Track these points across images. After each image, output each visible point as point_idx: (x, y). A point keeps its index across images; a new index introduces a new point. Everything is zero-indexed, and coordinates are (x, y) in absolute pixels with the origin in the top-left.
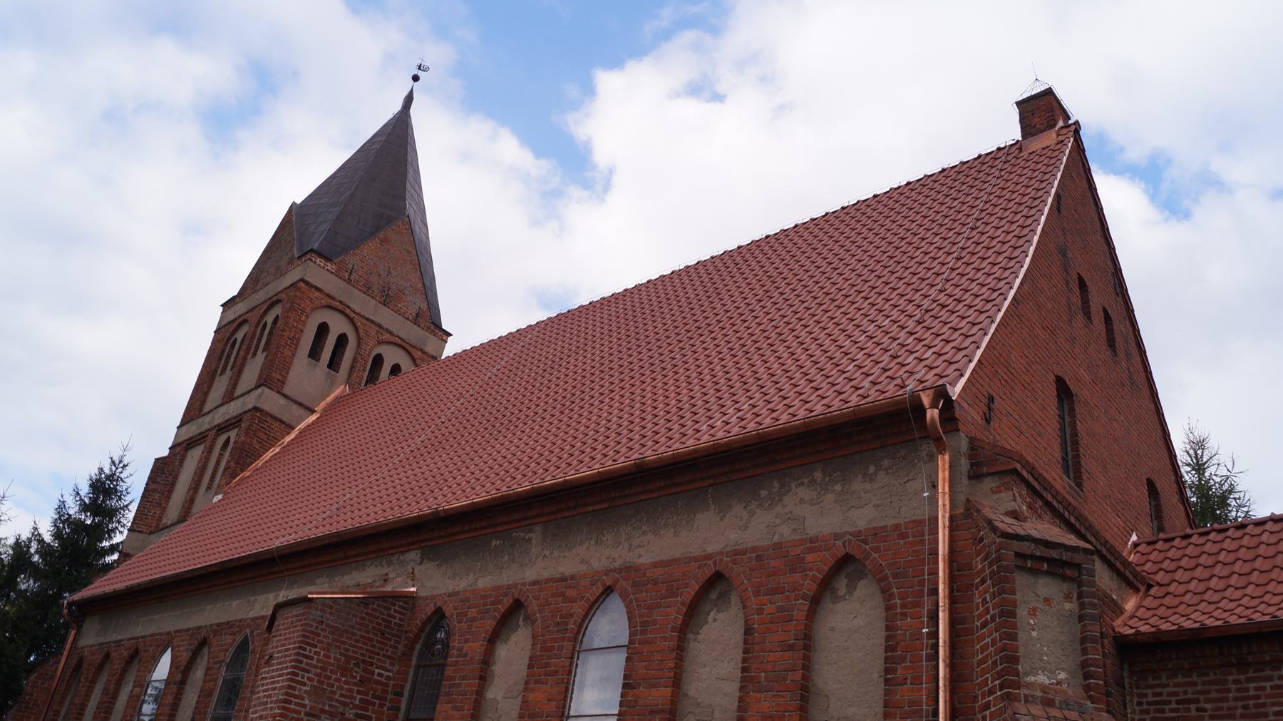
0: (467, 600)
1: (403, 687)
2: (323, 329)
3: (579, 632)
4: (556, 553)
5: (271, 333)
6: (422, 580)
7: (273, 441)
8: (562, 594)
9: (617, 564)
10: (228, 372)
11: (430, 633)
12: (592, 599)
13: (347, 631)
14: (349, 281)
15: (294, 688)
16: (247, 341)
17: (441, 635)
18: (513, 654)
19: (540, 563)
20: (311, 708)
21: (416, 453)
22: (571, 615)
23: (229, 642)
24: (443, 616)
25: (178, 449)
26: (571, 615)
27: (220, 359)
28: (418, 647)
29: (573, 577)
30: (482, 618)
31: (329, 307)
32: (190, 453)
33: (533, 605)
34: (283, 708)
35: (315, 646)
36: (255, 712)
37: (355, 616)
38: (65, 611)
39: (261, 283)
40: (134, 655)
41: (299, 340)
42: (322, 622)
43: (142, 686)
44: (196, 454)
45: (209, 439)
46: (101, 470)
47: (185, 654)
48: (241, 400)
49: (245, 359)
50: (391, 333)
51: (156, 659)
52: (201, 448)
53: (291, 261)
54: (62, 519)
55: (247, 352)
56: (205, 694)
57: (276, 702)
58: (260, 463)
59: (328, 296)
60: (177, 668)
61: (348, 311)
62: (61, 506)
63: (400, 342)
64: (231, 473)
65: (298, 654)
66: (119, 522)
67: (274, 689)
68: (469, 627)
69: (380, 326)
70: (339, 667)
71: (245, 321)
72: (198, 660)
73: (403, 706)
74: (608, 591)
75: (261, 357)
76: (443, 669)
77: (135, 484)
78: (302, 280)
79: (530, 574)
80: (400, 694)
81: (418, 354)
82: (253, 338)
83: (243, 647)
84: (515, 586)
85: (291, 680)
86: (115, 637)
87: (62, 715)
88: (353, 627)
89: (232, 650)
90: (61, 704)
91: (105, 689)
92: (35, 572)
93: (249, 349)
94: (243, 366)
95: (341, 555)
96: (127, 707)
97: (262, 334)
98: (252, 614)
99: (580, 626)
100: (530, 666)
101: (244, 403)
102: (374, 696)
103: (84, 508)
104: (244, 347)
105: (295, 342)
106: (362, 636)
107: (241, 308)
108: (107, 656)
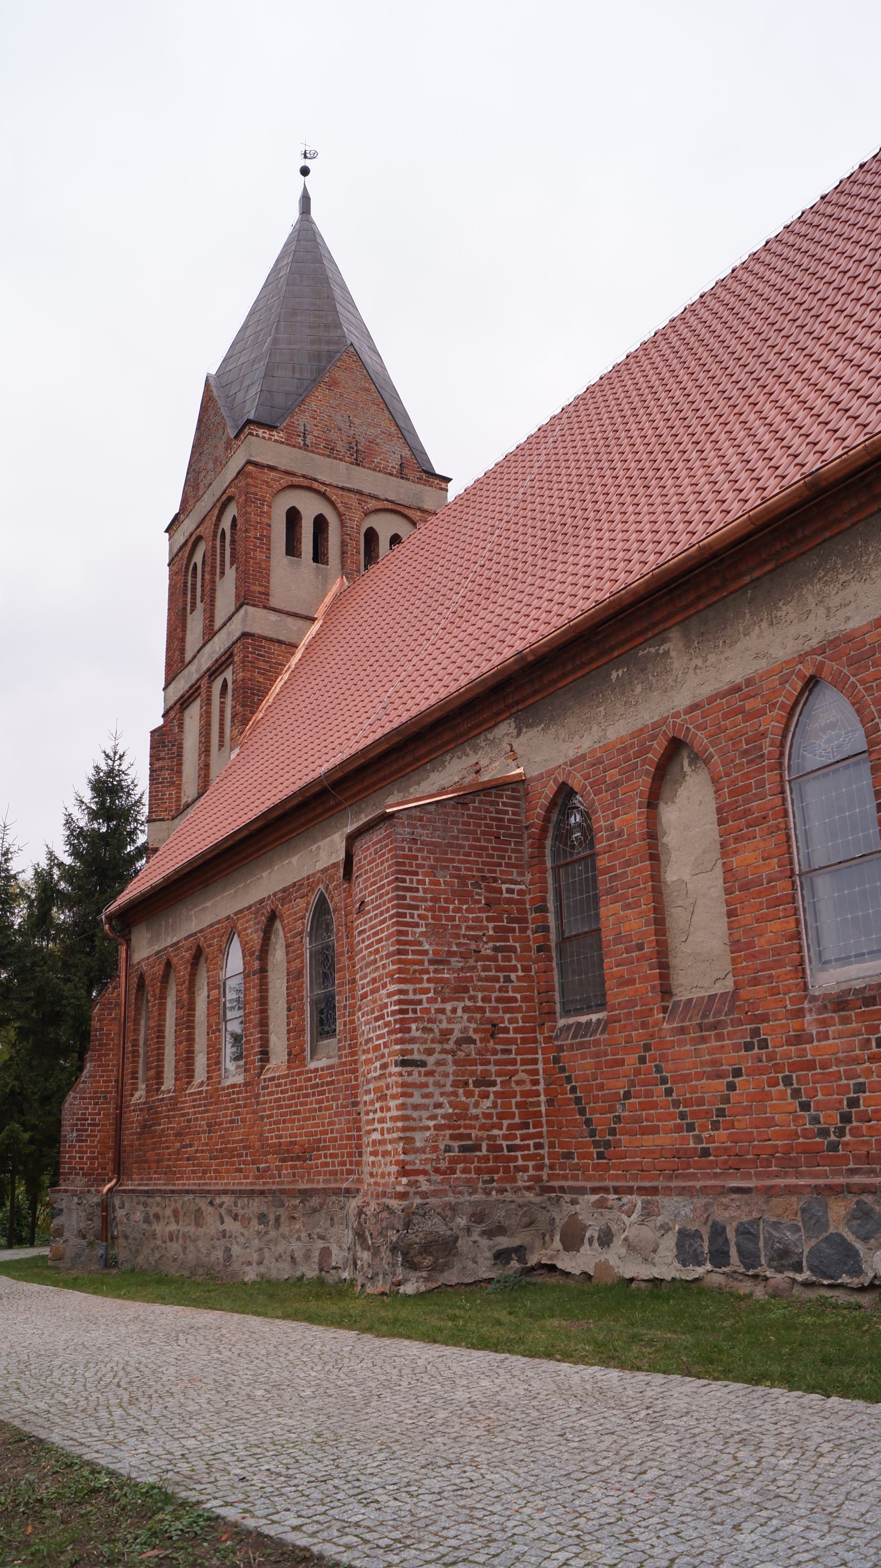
0: (600, 761)
1: (544, 899)
2: (293, 517)
3: (782, 754)
4: (712, 658)
5: (233, 542)
6: (530, 754)
7: (276, 669)
8: (741, 710)
9: (814, 643)
10: (200, 606)
11: (559, 822)
12: (790, 703)
13: (450, 845)
14: (306, 447)
15: (405, 933)
16: (209, 561)
17: (575, 819)
18: (690, 814)
19: (688, 679)
20: (435, 952)
21: (460, 611)
22: (763, 735)
23: (301, 910)
24: (572, 793)
25: (172, 714)
26: (763, 735)
27: (185, 594)
28: (548, 843)
29: (749, 682)
30: (629, 779)
31: (292, 487)
32: (187, 713)
33: (701, 739)
34: (400, 961)
35: (416, 874)
36: (365, 976)
37: (454, 823)
38: (107, 927)
39: (202, 486)
40: (198, 954)
41: (268, 538)
42: (415, 841)
43: (218, 987)
44: (194, 712)
45: (203, 689)
46: (97, 769)
47: (255, 936)
48: (224, 631)
49: (213, 582)
50: (377, 498)
51: (224, 952)
52: (198, 702)
53: (228, 446)
54: (76, 835)
55: (213, 574)
56: (294, 976)
57: (388, 956)
58: (270, 698)
59: (287, 473)
60: (252, 954)
61: (315, 485)
62: (69, 822)
63: (390, 506)
64: (242, 719)
65: (397, 888)
66: (136, 821)
67: (379, 941)
68: (614, 796)
69: (359, 492)
70: (454, 892)
71: (199, 538)
72: (273, 939)
73: (552, 923)
74: (811, 683)
75: (231, 573)
76: (594, 861)
77: (138, 774)
78: (249, 462)
79: (682, 700)
80: (543, 909)
81: (416, 515)
82: (214, 554)
83: (322, 908)
84: (665, 720)
85: (398, 906)
86: (170, 940)
87: (141, 1043)
88: (457, 838)
89: (309, 916)
90: (136, 1031)
91: (177, 1002)
92: (66, 901)
93: (213, 570)
94: (213, 590)
95: (408, 759)
96: (208, 1015)
97: (223, 547)
98: (320, 866)
99: (782, 745)
100: (721, 821)
101: (229, 634)
102: (511, 920)
103: (94, 815)
104: (208, 569)
105: (265, 541)
106: (470, 847)
107: (188, 526)
108: (168, 965)
